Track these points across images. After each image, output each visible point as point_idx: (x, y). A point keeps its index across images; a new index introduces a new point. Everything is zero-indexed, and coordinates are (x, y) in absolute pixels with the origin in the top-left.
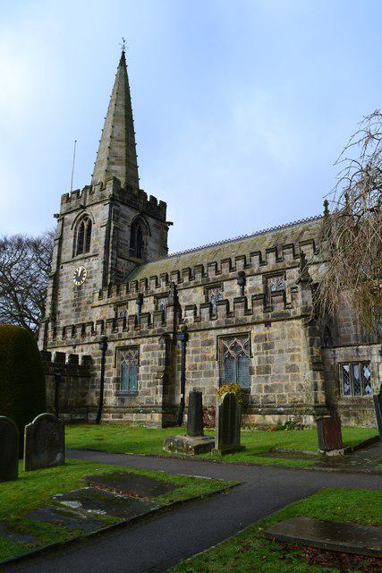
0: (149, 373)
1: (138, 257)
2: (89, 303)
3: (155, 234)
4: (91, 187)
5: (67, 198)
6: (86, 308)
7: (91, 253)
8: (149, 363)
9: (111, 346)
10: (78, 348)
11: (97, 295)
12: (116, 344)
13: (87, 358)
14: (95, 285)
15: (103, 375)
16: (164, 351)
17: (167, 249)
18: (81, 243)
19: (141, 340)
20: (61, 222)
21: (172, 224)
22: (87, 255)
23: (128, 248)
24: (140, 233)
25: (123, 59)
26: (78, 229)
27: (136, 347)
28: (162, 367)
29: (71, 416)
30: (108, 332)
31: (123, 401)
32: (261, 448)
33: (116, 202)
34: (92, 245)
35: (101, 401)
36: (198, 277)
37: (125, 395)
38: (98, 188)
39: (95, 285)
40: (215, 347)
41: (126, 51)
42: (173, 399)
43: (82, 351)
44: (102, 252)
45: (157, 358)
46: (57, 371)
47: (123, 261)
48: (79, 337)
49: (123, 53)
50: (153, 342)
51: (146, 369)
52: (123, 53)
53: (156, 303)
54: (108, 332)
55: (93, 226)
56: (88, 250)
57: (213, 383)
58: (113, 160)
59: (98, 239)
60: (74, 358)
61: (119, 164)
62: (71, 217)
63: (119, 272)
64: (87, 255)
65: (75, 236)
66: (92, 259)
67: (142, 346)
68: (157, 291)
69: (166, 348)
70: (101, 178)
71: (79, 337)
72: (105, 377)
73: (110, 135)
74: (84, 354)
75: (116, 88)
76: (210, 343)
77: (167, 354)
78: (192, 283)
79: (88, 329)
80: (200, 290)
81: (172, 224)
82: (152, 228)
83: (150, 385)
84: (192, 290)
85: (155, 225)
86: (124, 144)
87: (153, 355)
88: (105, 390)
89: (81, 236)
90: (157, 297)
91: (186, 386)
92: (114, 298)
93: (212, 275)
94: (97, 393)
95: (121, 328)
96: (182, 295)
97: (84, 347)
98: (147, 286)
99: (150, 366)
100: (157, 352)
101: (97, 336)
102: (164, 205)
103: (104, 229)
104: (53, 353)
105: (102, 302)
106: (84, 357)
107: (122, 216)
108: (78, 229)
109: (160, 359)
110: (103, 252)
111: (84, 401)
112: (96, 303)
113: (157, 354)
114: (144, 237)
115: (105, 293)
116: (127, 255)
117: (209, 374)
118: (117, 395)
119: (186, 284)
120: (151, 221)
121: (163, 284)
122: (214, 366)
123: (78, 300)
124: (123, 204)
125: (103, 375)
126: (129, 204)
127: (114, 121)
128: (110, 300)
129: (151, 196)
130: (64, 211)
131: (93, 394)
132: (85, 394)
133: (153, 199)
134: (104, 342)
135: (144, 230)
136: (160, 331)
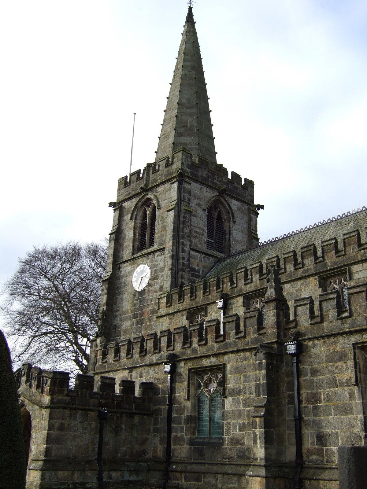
0: (242, 408)
1: (218, 251)
2: (153, 312)
3: (241, 220)
4: (155, 164)
5: (124, 183)
6: (150, 320)
7: (156, 247)
8: (239, 393)
9: (183, 368)
10: (134, 373)
11: (164, 300)
12: (190, 365)
13: (147, 387)
14: (161, 288)
15: (170, 411)
16: (264, 372)
17: (258, 239)
18: (143, 235)
19: (226, 357)
20: (117, 212)
21: (262, 207)
22: (150, 250)
23: (205, 238)
24: (220, 218)
25: (190, 20)
26: (139, 218)
27: (221, 368)
28: (263, 398)
29: (122, 476)
30: (178, 348)
31: (201, 453)
32: (357, 264)
33: (187, 180)
34: (156, 237)
35: (168, 451)
36: (309, 262)
37: (204, 444)
38: (163, 164)
39: (161, 288)
40: (350, 363)
41: (194, 5)
42: (280, 453)
43: (141, 376)
44: (169, 244)
45: (253, 384)
46: (100, 405)
47: (198, 255)
48: (136, 356)
49: (190, 8)
50: (245, 359)
51: (236, 403)
52: (190, 8)
53: (246, 304)
54: (178, 348)
55: (158, 213)
56: (151, 243)
57: (351, 425)
58: (182, 130)
59: (164, 228)
60: (128, 385)
61: (189, 136)
62: (129, 205)
63: (193, 269)
64: (150, 250)
65: (135, 228)
66: (157, 254)
67: (229, 366)
68: (250, 288)
69: (267, 368)
70: (169, 152)
71: (136, 356)
72: (174, 415)
73: (178, 101)
74: (144, 380)
75: (183, 47)
76: (342, 357)
77: (269, 376)
78: (300, 273)
79: (149, 345)
80: (313, 282)
81: (262, 207)
82: (237, 215)
83: (243, 427)
84: (299, 283)
85: (239, 209)
86: (194, 110)
87: (247, 379)
88: (173, 434)
89: (143, 226)
90: (248, 299)
91: (304, 431)
92: (187, 303)
93: (331, 260)
94: (161, 439)
95: (195, 341)
96: (288, 289)
97: (144, 370)
98: (232, 283)
99: (241, 397)
100: (252, 374)
101: (162, 353)
102: (250, 184)
103: (172, 214)
104: (97, 378)
105: (171, 310)
106: (143, 384)
107: (195, 197)
108: (139, 218)
109: (258, 386)
110: (171, 243)
111: (144, 452)
112: (163, 311)
113: (253, 378)
114: (226, 225)
115: (175, 297)
116: (203, 247)
117: (345, 410)
118: (191, 443)
119: (290, 275)
120: (235, 204)
121: (256, 278)
122: (352, 396)
123: (139, 309)
124: (196, 181)
125: (170, 411)
126: (203, 182)
127: (181, 85)
128: (181, 307)
129: (233, 173)
130: (122, 198)
131: (157, 440)
132: (144, 441)
133: (236, 176)
134: (173, 360)
135: (225, 216)
136: (255, 341)
